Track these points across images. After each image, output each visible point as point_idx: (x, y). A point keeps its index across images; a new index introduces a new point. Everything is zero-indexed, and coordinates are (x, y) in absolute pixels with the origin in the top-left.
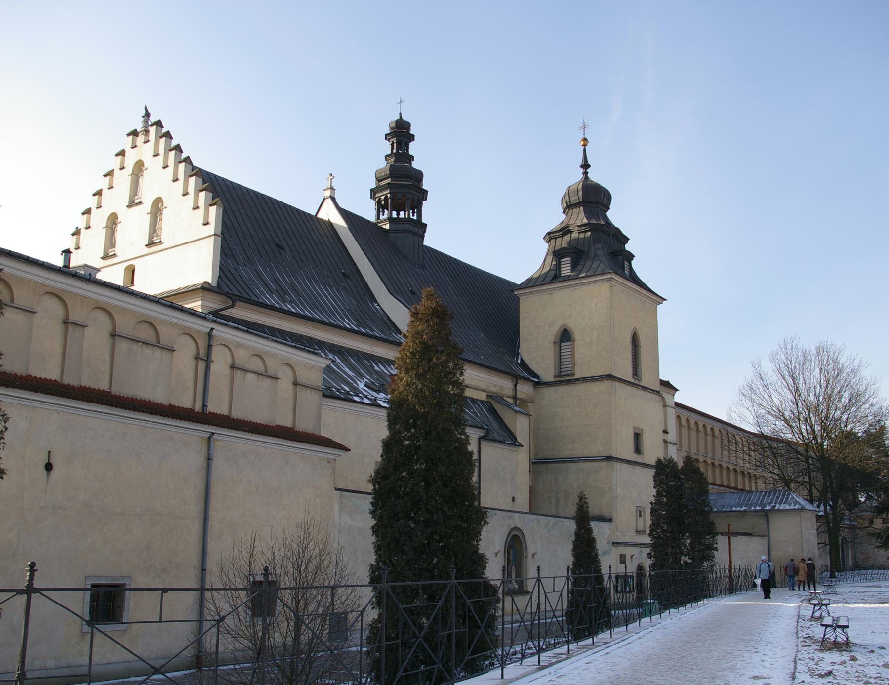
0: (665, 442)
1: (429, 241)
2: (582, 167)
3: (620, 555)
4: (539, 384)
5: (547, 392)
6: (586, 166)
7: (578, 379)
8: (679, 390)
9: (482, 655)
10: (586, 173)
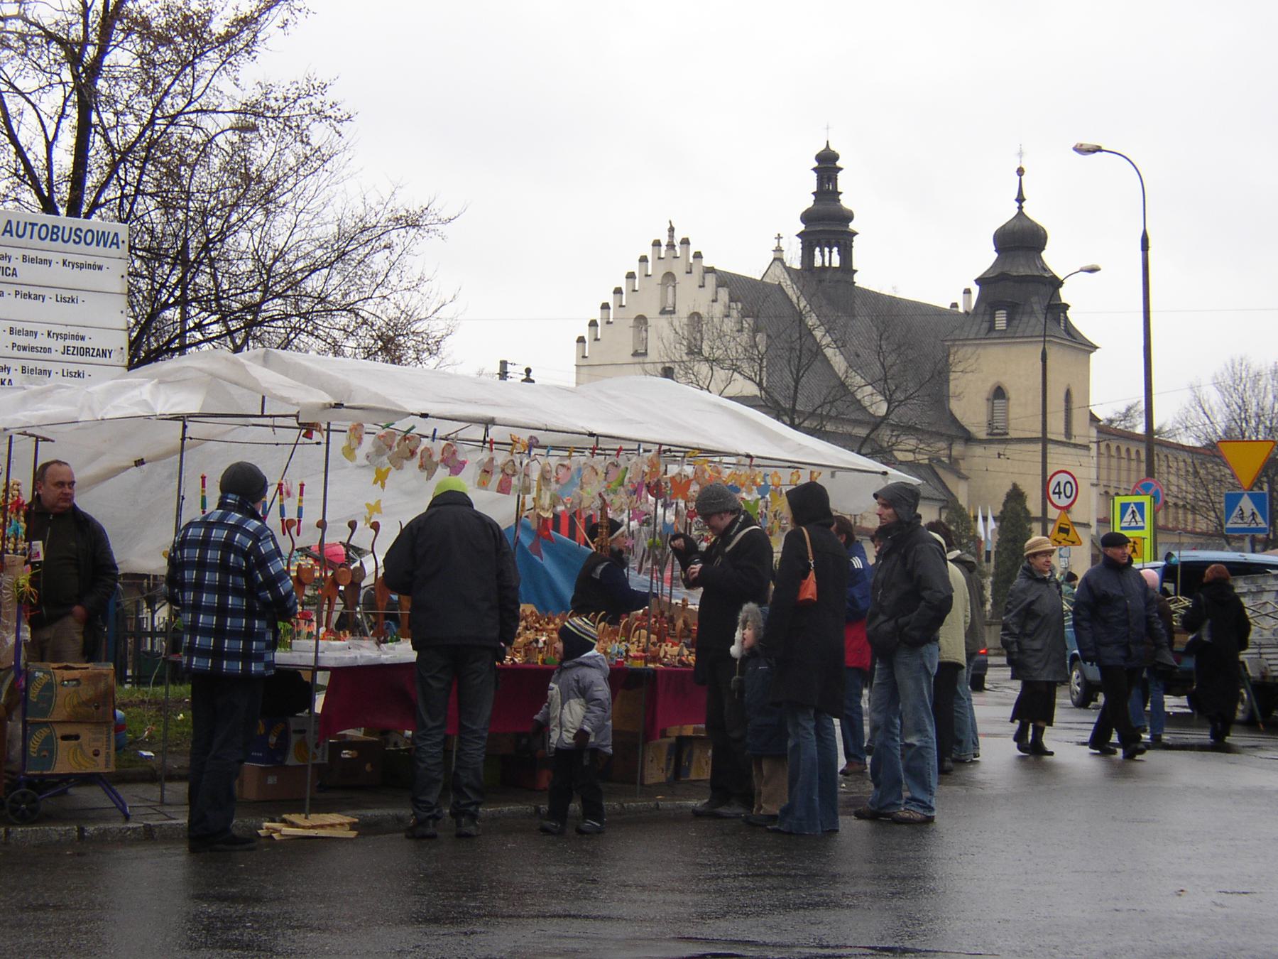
1: (856, 285)
2: (1017, 200)
4: (969, 439)
5: (978, 450)
6: (1020, 199)
7: (1012, 440)
8: (856, 234)
10: (1020, 208)
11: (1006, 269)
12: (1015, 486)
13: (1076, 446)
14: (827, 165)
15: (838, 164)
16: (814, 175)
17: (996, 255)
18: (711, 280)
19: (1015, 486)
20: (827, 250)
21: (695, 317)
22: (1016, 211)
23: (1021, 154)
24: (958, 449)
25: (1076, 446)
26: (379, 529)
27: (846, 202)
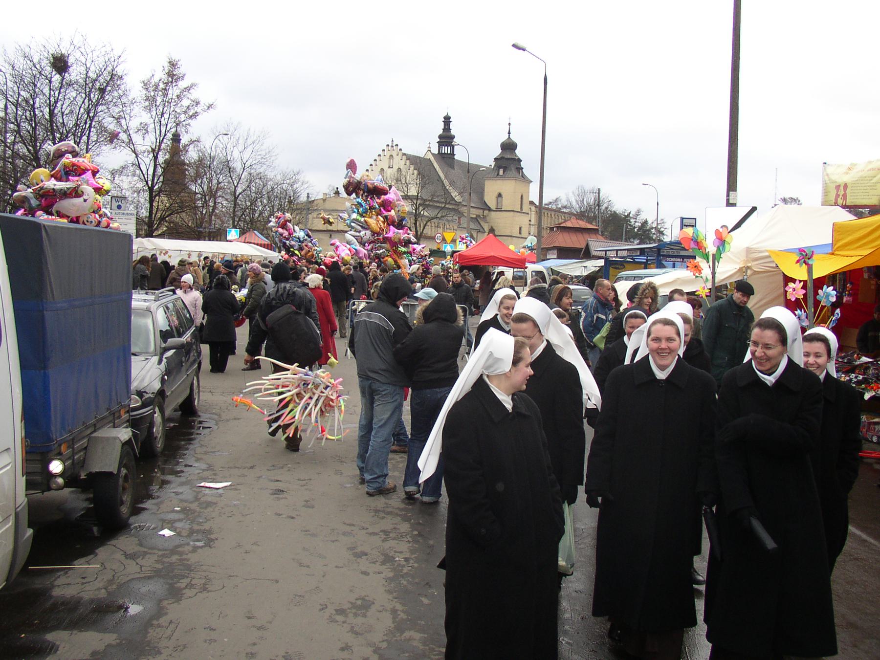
0: (530, 224)
3: (822, 205)
4: (490, 209)
5: (493, 213)
6: (509, 133)
9: (626, 235)
11: (503, 156)
12: (340, 650)
13: (523, 213)
14: (447, 120)
15: (451, 120)
16: (443, 123)
17: (501, 151)
18: (404, 157)
19: (340, 650)
20: (446, 147)
21: (399, 170)
22: (508, 137)
23: (510, 119)
24: (486, 212)
25: (523, 213)
26: (356, 170)
27: (453, 132)
